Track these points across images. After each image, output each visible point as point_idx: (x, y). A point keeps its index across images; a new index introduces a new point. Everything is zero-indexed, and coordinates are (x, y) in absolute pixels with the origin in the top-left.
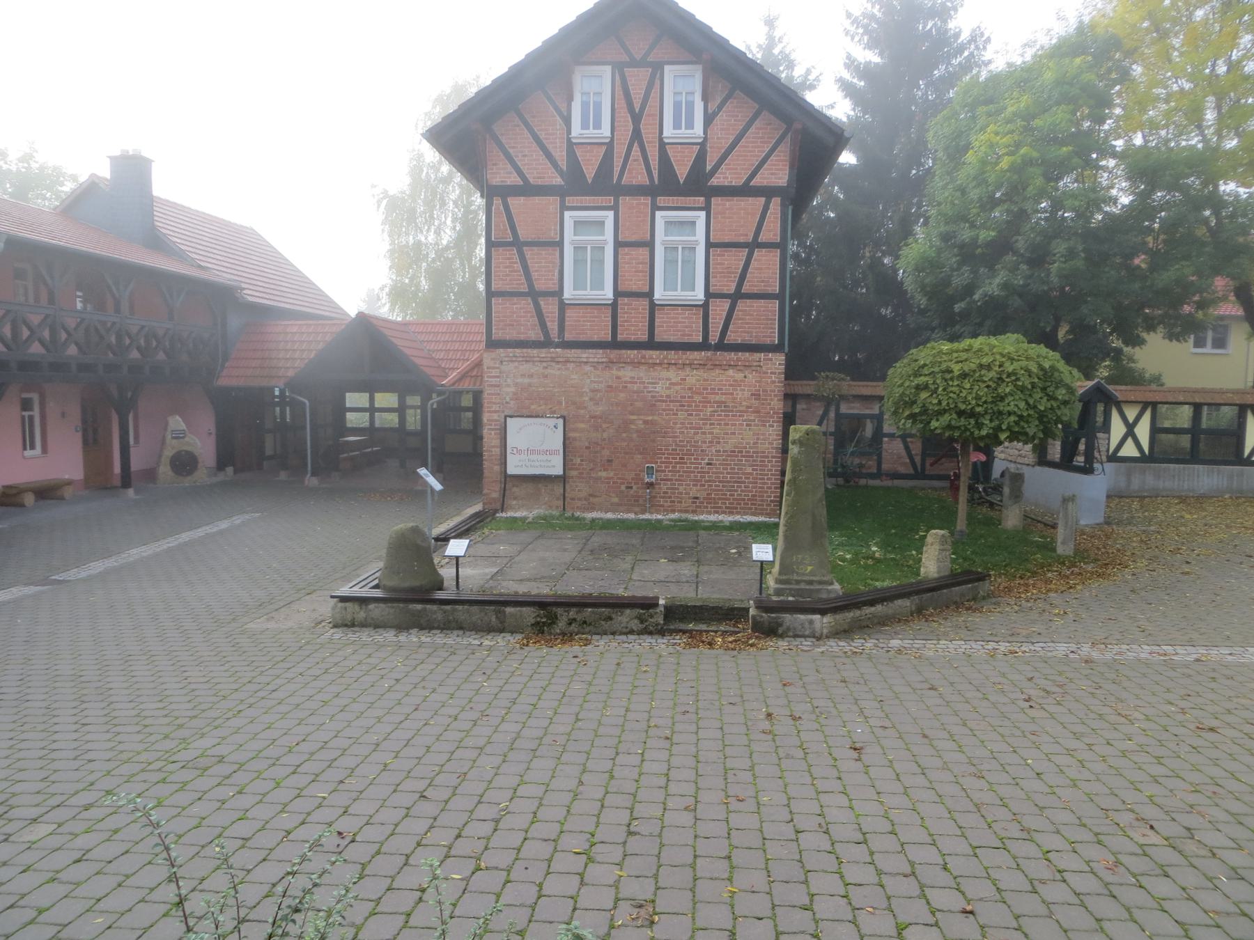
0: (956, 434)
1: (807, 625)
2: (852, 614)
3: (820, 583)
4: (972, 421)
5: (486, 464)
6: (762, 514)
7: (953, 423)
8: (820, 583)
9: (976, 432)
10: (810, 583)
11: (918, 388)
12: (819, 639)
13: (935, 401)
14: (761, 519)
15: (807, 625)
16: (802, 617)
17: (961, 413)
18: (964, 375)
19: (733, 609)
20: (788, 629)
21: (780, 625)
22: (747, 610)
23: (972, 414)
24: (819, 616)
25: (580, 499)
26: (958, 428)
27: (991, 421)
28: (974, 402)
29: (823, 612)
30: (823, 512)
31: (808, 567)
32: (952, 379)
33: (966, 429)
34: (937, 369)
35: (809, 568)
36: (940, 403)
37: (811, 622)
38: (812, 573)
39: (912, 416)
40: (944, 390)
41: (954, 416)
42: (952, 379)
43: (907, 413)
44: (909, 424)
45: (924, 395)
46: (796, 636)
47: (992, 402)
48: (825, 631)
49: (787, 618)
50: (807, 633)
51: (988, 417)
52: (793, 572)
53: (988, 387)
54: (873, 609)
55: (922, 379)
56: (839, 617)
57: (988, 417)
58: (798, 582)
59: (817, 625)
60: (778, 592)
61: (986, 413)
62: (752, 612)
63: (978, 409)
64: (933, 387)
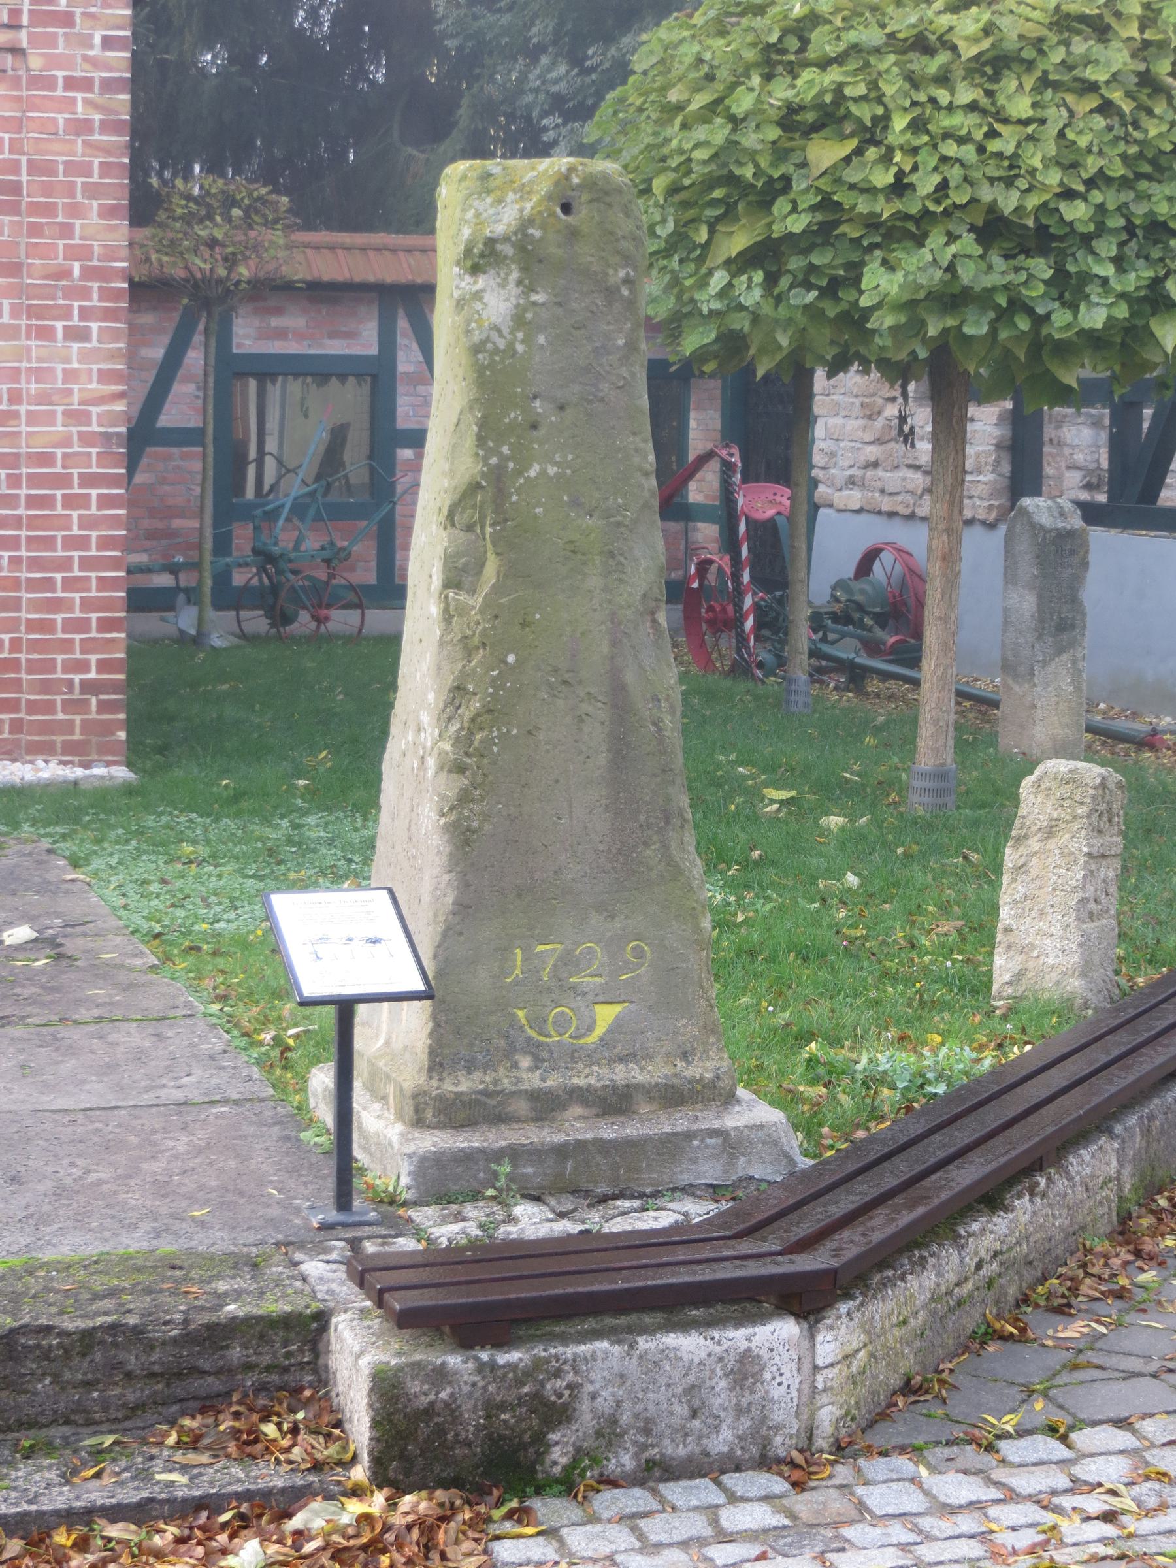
0: (976, 326)
1: (720, 1393)
2: (930, 1279)
3: (673, 1096)
4: (1042, 268)
5: (739, 1323)
6: (44, 750)
7: (967, 273)
8: (673, 1096)
9: (1061, 317)
10: (615, 1102)
11: (791, 119)
12: (800, 1470)
13: (883, 178)
14: (46, 771)
15: (720, 1393)
16: (689, 1345)
17: (993, 229)
18: (995, 65)
19: (218, 1335)
20: (609, 1431)
21: (556, 1414)
22: (312, 1328)
23: (1041, 237)
24: (787, 1329)
25: (57, 1292)
26: (984, 298)
27: (1119, 262)
28: (1053, 178)
29: (805, 1300)
30: (660, 675)
31: (590, 1014)
32: (943, 79)
33: (1018, 305)
34: (872, 36)
35: (606, 1015)
36: (900, 187)
37: (746, 1370)
38: (621, 1046)
39: (765, 256)
40: (917, 126)
41: (968, 243)
42: (943, 79)
43: (738, 241)
44: (751, 291)
45: (825, 153)
46: (656, 1472)
47: (1125, 183)
48: (827, 1415)
49: (602, 1366)
50: (721, 1441)
51: (1107, 247)
52: (512, 1047)
53: (1106, 108)
54: (1001, 1223)
55: (811, 84)
56: (884, 1308)
57: (1107, 247)
58: (547, 1106)
59: (783, 1387)
60: (443, 1183)
61: (1101, 230)
62: (358, 1354)
63: (1077, 212)
64: (865, 113)
